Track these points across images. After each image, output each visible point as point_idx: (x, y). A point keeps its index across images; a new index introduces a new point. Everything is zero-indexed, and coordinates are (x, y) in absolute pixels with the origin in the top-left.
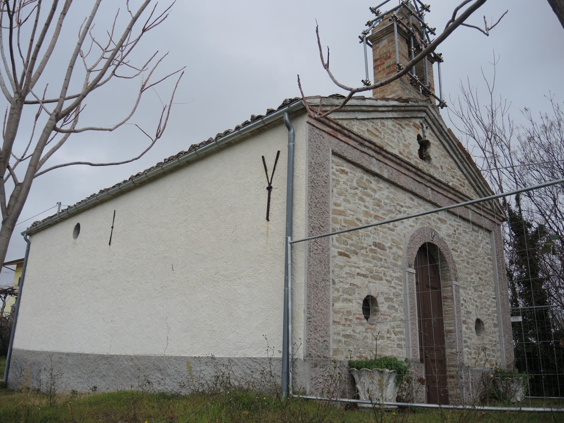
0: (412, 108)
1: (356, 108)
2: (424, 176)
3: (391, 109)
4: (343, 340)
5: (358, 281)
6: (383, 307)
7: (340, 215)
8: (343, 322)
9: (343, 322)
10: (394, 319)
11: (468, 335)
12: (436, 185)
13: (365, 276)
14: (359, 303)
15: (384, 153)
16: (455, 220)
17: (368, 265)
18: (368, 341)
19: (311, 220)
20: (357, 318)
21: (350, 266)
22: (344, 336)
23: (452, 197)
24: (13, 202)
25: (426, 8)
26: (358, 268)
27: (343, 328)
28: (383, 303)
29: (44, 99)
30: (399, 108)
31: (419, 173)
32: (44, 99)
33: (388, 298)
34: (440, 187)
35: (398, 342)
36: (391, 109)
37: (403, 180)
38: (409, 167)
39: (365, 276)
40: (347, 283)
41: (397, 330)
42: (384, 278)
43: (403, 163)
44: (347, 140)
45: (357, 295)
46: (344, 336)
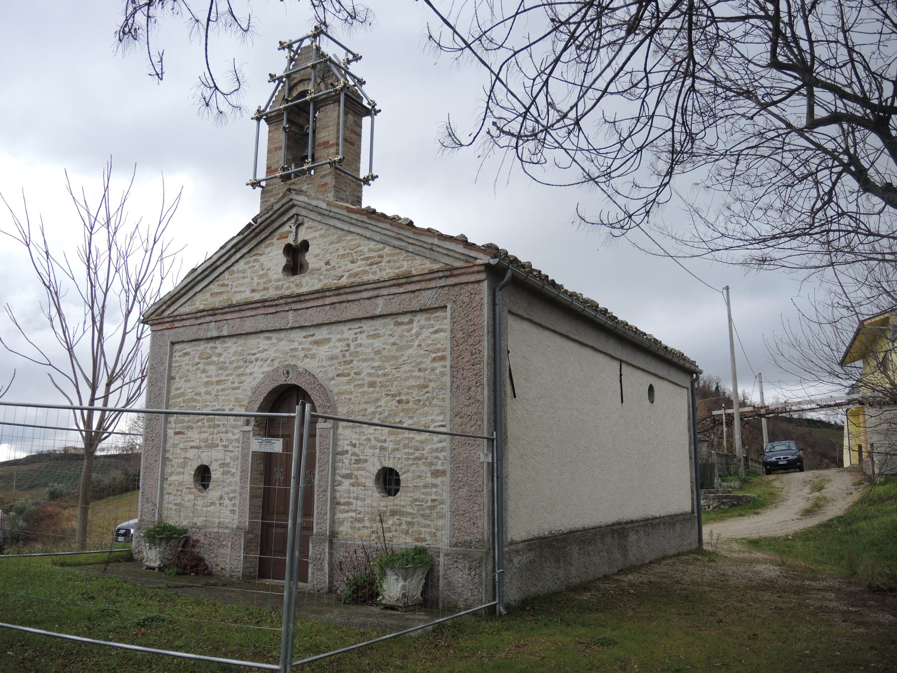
0: (265, 224)
1: (192, 283)
2: (277, 302)
3: (234, 250)
4: (174, 507)
5: (191, 454)
6: (216, 475)
7: (179, 397)
8: (175, 492)
9: (175, 492)
10: (230, 484)
11: (355, 495)
12: (300, 301)
13: (198, 448)
14: (190, 474)
15: (219, 311)
16: (350, 329)
17: (203, 436)
18: (198, 508)
19: (317, 383)
20: (187, 488)
21: (184, 442)
22: (175, 504)
23: (335, 299)
24: (641, 523)
25: (272, 78)
26: (193, 441)
27: (174, 497)
28: (216, 470)
29: (524, 106)
30: (246, 240)
31: (267, 304)
32: (524, 106)
33: (223, 464)
34: (305, 300)
35: (232, 508)
36: (234, 250)
37: (249, 325)
38: (251, 306)
39: (198, 448)
40: (181, 458)
41: (231, 495)
42: (220, 444)
43: (242, 308)
44: (184, 323)
45: (189, 467)
46: (175, 504)
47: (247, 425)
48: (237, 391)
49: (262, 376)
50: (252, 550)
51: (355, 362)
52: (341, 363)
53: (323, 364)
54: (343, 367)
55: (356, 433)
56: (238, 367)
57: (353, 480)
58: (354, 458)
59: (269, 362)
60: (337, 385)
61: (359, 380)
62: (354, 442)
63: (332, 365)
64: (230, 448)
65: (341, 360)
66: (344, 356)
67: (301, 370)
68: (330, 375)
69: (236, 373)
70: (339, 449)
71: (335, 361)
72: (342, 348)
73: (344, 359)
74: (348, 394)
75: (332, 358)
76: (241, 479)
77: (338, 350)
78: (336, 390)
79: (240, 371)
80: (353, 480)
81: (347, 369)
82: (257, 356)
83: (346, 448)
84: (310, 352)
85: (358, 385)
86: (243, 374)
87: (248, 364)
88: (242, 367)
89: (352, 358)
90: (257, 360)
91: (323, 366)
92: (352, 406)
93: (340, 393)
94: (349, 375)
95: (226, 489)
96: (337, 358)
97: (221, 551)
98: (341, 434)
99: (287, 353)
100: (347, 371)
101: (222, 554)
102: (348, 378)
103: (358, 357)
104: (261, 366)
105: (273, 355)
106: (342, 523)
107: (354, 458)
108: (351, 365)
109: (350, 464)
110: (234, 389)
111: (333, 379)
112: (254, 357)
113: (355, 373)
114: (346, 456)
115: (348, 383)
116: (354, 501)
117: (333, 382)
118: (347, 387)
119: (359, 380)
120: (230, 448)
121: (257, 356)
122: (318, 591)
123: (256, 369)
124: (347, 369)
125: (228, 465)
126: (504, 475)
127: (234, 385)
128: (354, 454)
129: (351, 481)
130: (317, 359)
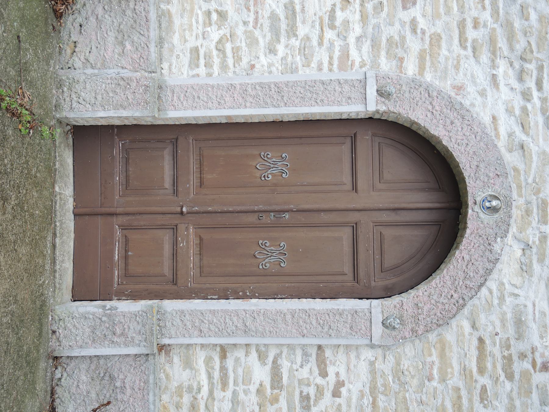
47: (381, 93)
48: (456, 41)
49: (487, 120)
50: (46, 244)
51: (508, 385)
52: (508, 347)
53: (508, 300)
54: (498, 355)
55: (362, 395)
56: (511, 38)
57: (269, 391)
58: (312, 391)
59: (520, 136)
60: (460, 335)
61: (470, 401)
62: (344, 390)
63: (503, 321)
64: (329, 34)
65: (517, 347)
66: (522, 356)
67: (497, 247)
68: (482, 319)
69: (499, 31)
70: (328, 353)
71: (511, 331)
72: (540, 350)
73: (515, 358)
74: (440, 369)
75: (519, 323)
76: (261, 85)
77: (536, 340)
78: (450, 336)
79: (502, 43)
80: (269, 391)
81: (494, 366)
82: (535, 94)
83: (331, 370)
84: (535, 258)
85: (459, 397)
86: (494, 53)
87: (517, 65)
88: (512, 49)
89: (517, 376)
90: (526, 96)
91: (502, 299)
92: (415, 382)
93: (443, 350)
94: (481, 370)
95: (240, 30)
96: (520, 337)
97: (111, 37)
98: (358, 357)
99: (537, 192)
100: (489, 365)
101: (104, 39)
102: (475, 370)
103: (519, 394)
104: (510, 111)
105: (534, 149)
106: (188, 364)
107: (312, 391)
108: (502, 378)
109: (300, 382)
110: (462, 25)
111: (474, 326)
112: (531, 84)
113: (484, 389)
114: (316, 371)
115: (465, 371)
116: (229, 394)
117: (466, 325)
118: (456, 367)
119: (470, 401)
120: (329, 34)
121: (535, 94)
122: (54, 332)
123: (505, 93)
124: (494, 366)
125: (292, 31)
126: (408, 125)
127: (469, 24)
128: (320, 391)
129: (268, 387)
130: (517, 281)
